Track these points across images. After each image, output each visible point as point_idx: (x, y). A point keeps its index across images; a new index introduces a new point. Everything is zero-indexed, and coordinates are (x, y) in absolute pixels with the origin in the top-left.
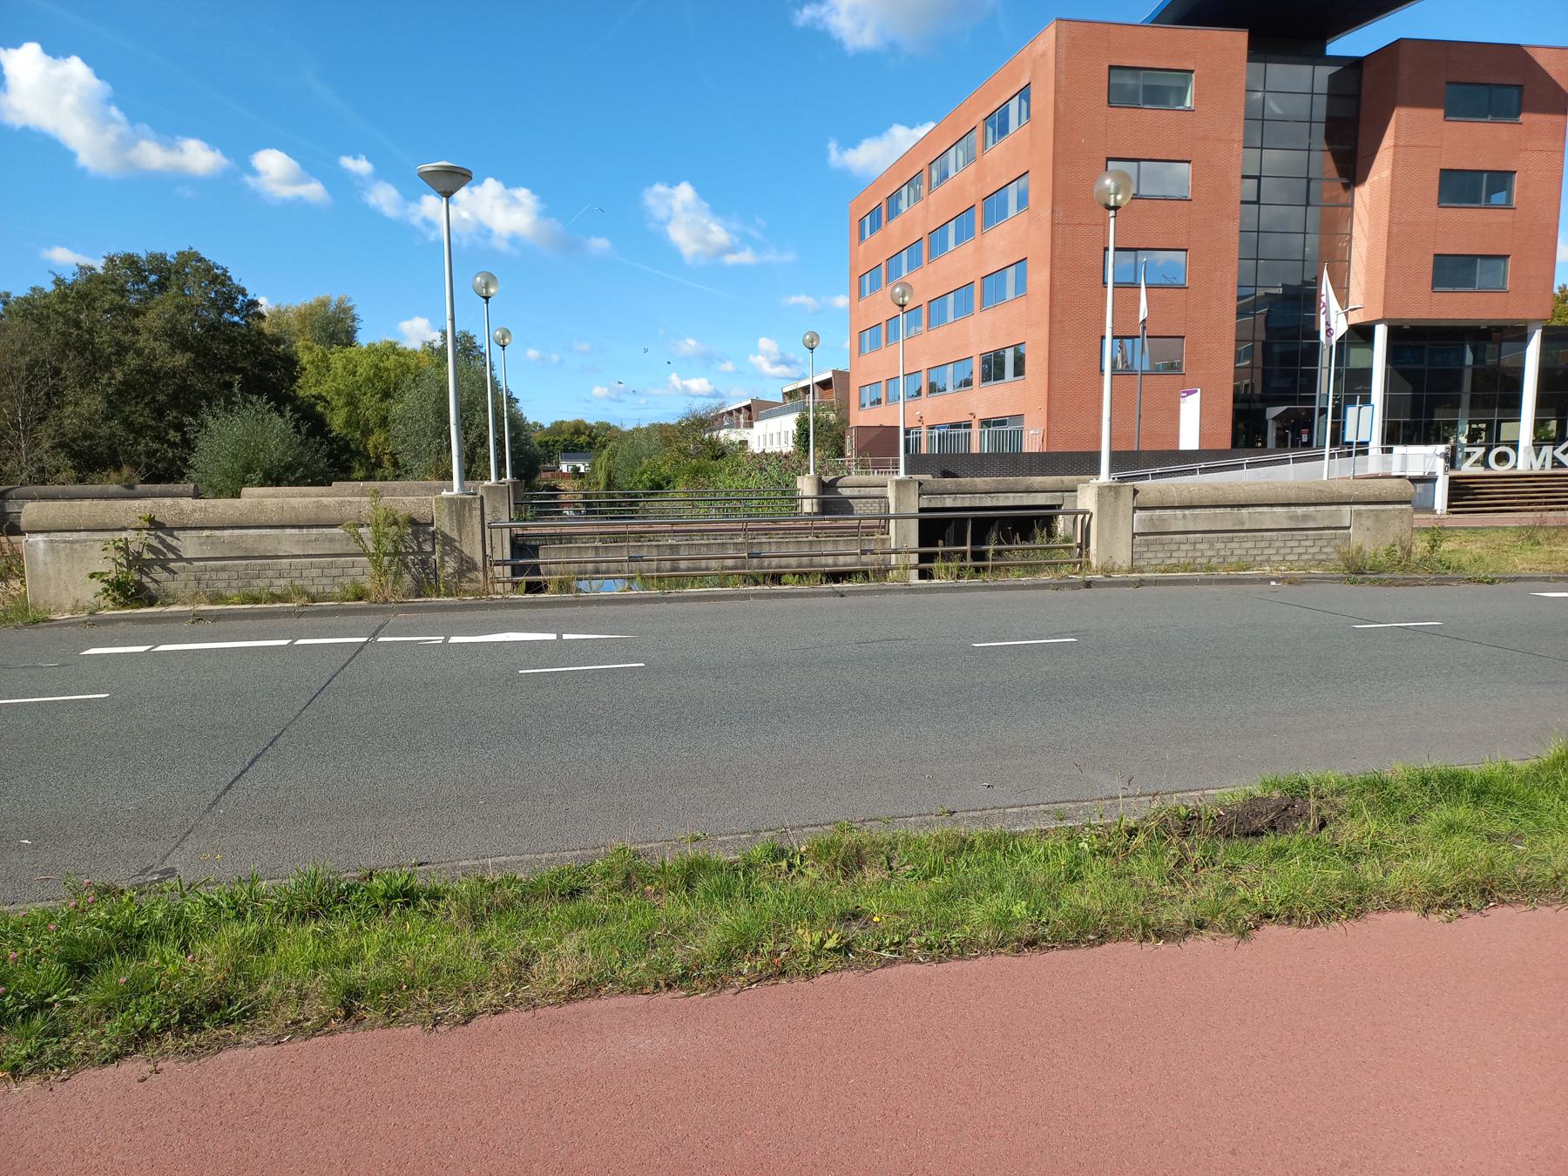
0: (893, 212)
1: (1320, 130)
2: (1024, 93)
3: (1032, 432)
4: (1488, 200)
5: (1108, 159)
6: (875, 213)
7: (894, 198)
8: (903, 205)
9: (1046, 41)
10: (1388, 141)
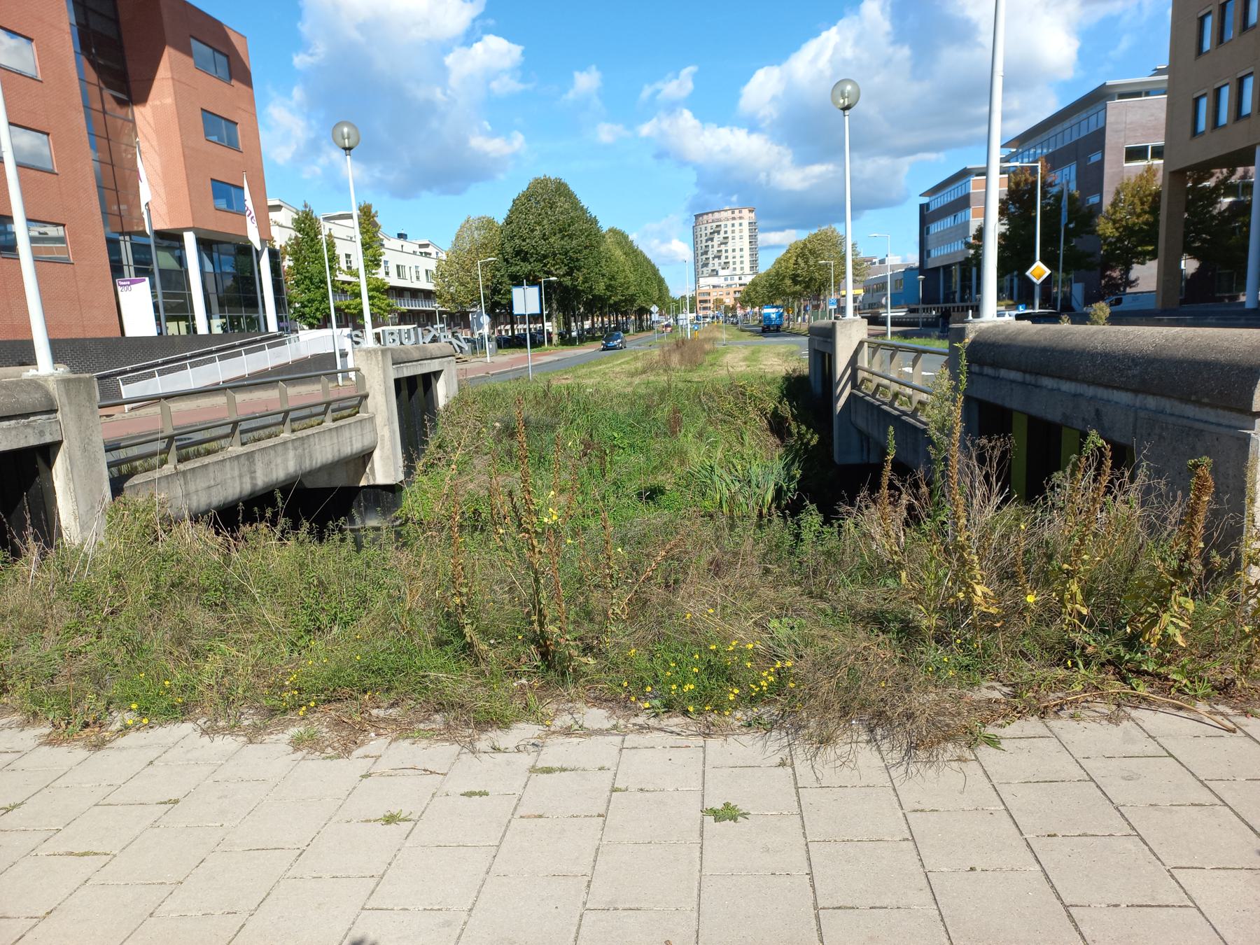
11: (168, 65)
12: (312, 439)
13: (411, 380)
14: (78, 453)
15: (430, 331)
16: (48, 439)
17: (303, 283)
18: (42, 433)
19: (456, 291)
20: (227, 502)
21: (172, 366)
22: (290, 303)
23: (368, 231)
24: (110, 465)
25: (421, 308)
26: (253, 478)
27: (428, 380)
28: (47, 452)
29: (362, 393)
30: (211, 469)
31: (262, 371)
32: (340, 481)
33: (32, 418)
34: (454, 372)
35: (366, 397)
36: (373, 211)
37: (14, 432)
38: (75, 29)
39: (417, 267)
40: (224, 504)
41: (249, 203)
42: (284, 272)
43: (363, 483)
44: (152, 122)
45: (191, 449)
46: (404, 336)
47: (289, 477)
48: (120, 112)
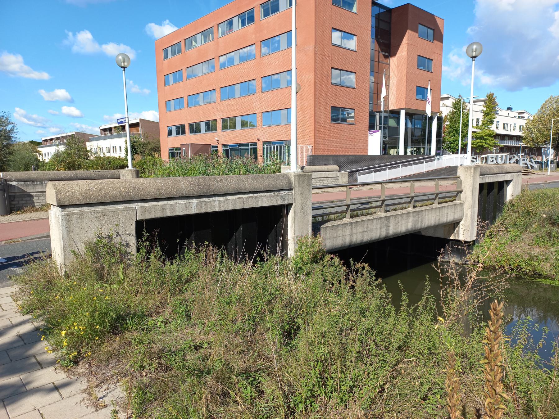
3: (309, 147)
10: (405, 41)
11: (407, 38)
12: (424, 213)
13: (491, 185)
14: (299, 210)
15: (514, 157)
16: (286, 202)
17: (452, 132)
18: (284, 199)
19: (536, 136)
20: (372, 240)
21: (381, 169)
22: (444, 142)
23: (490, 106)
24: (313, 217)
25: (513, 145)
26: (387, 230)
27: (502, 185)
28: (288, 207)
29: (459, 190)
30: (366, 223)
31: (429, 171)
32: (440, 234)
33: (281, 192)
34: (520, 181)
35: (461, 192)
36: (494, 96)
37: (272, 198)
38: (374, 30)
39: (515, 124)
40: (370, 241)
41: (429, 95)
42: (444, 127)
43: (452, 238)
44: (396, 64)
45: (359, 212)
46: (499, 159)
47: (407, 231)
48: (385, 61)
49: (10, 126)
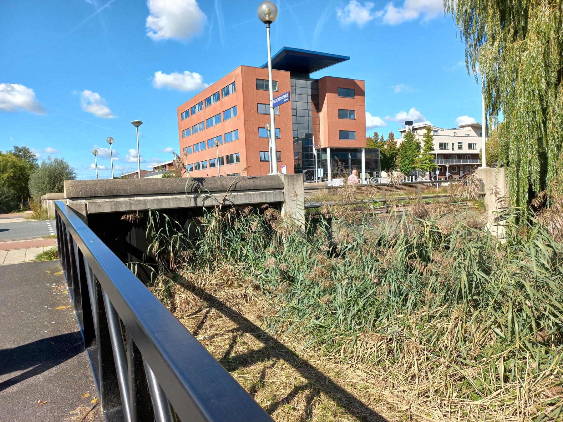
0: (193, 112)
1: (310, 97)
2: (233, 84)
4: (350, 117)
5: (258, 104)
6: (187, 112)
7: (193, 108)
8: (196, 110)
9: (239, 71)
10: (326, 101)
49: (74, 175)
